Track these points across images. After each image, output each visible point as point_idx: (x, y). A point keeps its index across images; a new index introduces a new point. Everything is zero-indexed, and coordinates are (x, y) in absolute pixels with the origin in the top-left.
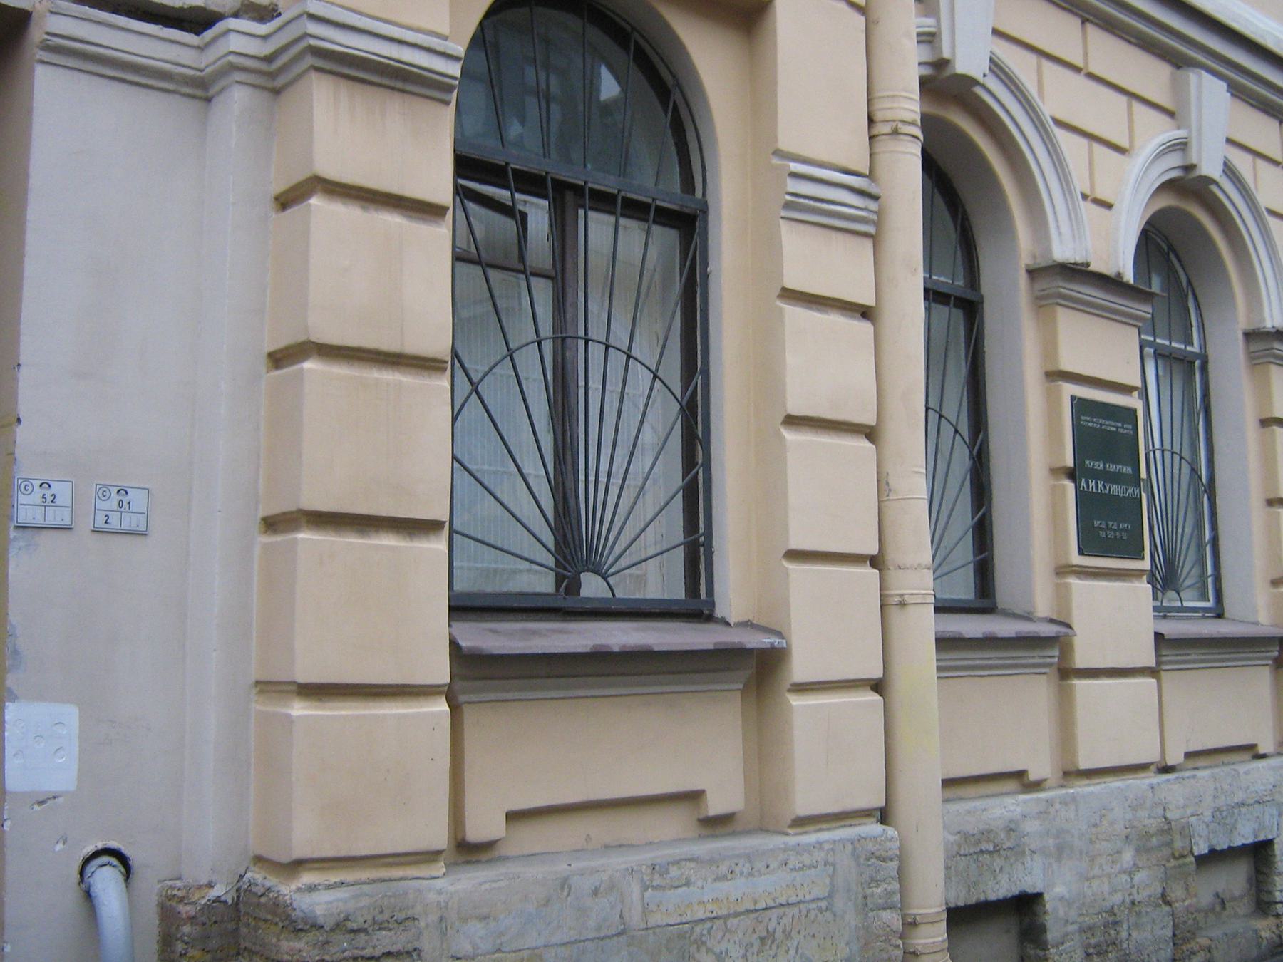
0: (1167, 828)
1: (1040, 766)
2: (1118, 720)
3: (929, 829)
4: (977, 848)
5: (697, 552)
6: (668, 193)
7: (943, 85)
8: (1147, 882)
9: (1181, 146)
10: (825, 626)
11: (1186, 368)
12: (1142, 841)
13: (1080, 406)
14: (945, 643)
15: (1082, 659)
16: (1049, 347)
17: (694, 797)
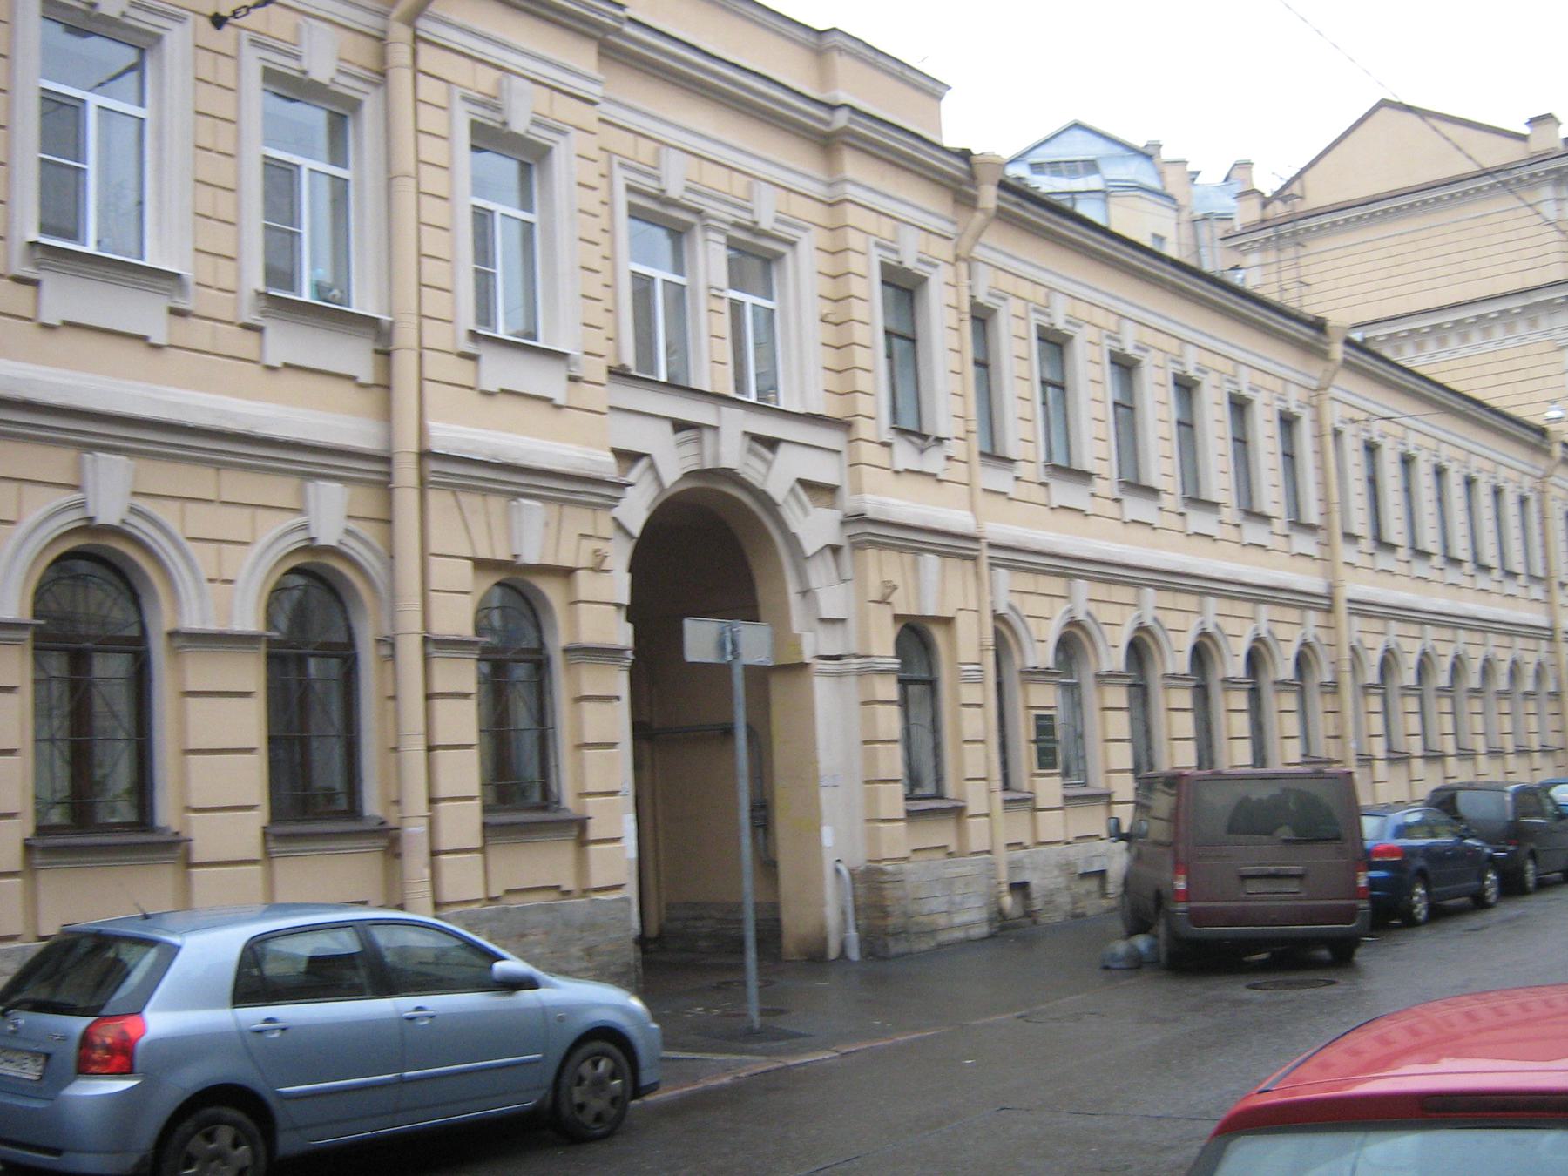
0: (1069, 864)
1: (1028, 841)
2: (1052, 825)
3: (1003, 856)
4: (1014, 866)
5: (939, 780)
6: (924, 675)
7: (998, 617)
8: (1061, 881)
9: (1070, 610)
10: (977, 799)
11: (1072, 691)
12: (1059, 866)
13: (1039, 718)
14: (1006, 801)
15: (196, 858)
16: (1026, 696)
17: (945, 847)
